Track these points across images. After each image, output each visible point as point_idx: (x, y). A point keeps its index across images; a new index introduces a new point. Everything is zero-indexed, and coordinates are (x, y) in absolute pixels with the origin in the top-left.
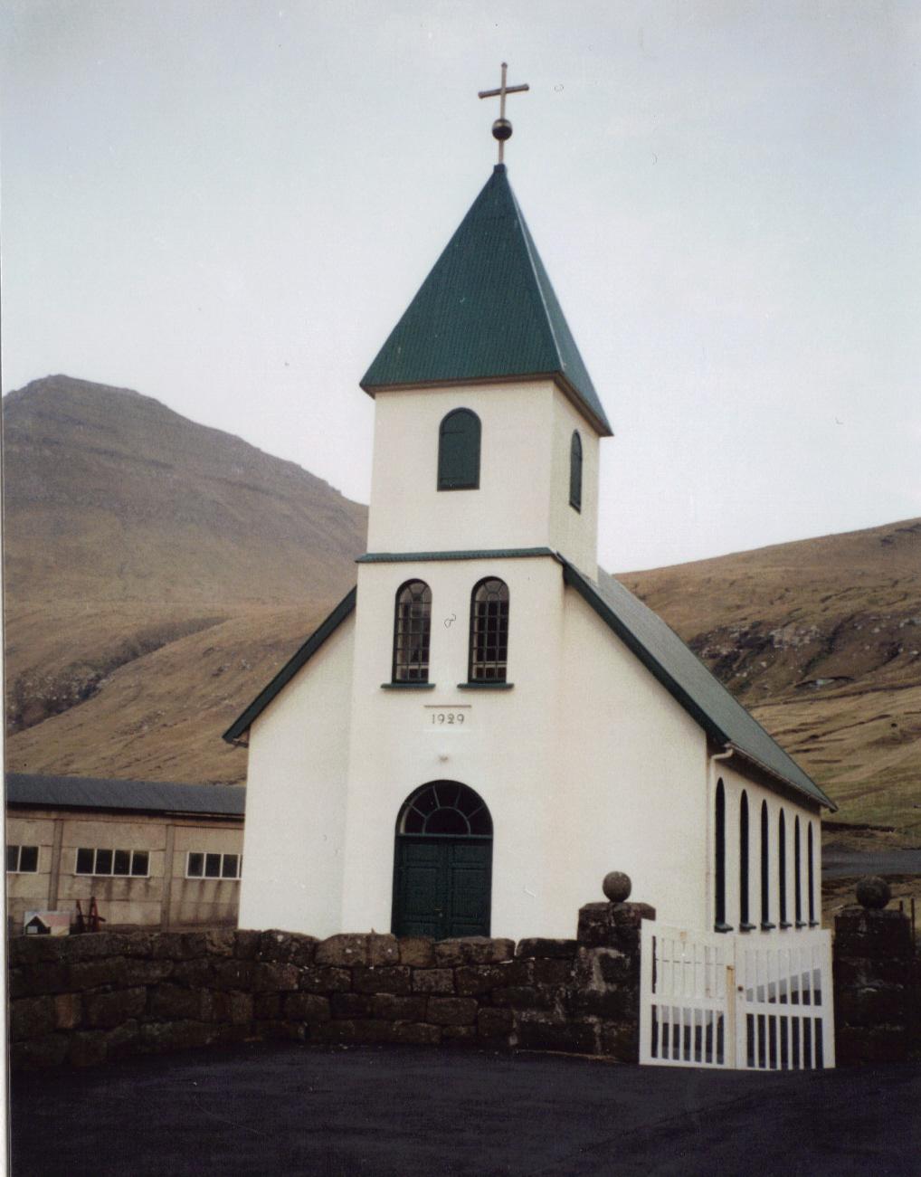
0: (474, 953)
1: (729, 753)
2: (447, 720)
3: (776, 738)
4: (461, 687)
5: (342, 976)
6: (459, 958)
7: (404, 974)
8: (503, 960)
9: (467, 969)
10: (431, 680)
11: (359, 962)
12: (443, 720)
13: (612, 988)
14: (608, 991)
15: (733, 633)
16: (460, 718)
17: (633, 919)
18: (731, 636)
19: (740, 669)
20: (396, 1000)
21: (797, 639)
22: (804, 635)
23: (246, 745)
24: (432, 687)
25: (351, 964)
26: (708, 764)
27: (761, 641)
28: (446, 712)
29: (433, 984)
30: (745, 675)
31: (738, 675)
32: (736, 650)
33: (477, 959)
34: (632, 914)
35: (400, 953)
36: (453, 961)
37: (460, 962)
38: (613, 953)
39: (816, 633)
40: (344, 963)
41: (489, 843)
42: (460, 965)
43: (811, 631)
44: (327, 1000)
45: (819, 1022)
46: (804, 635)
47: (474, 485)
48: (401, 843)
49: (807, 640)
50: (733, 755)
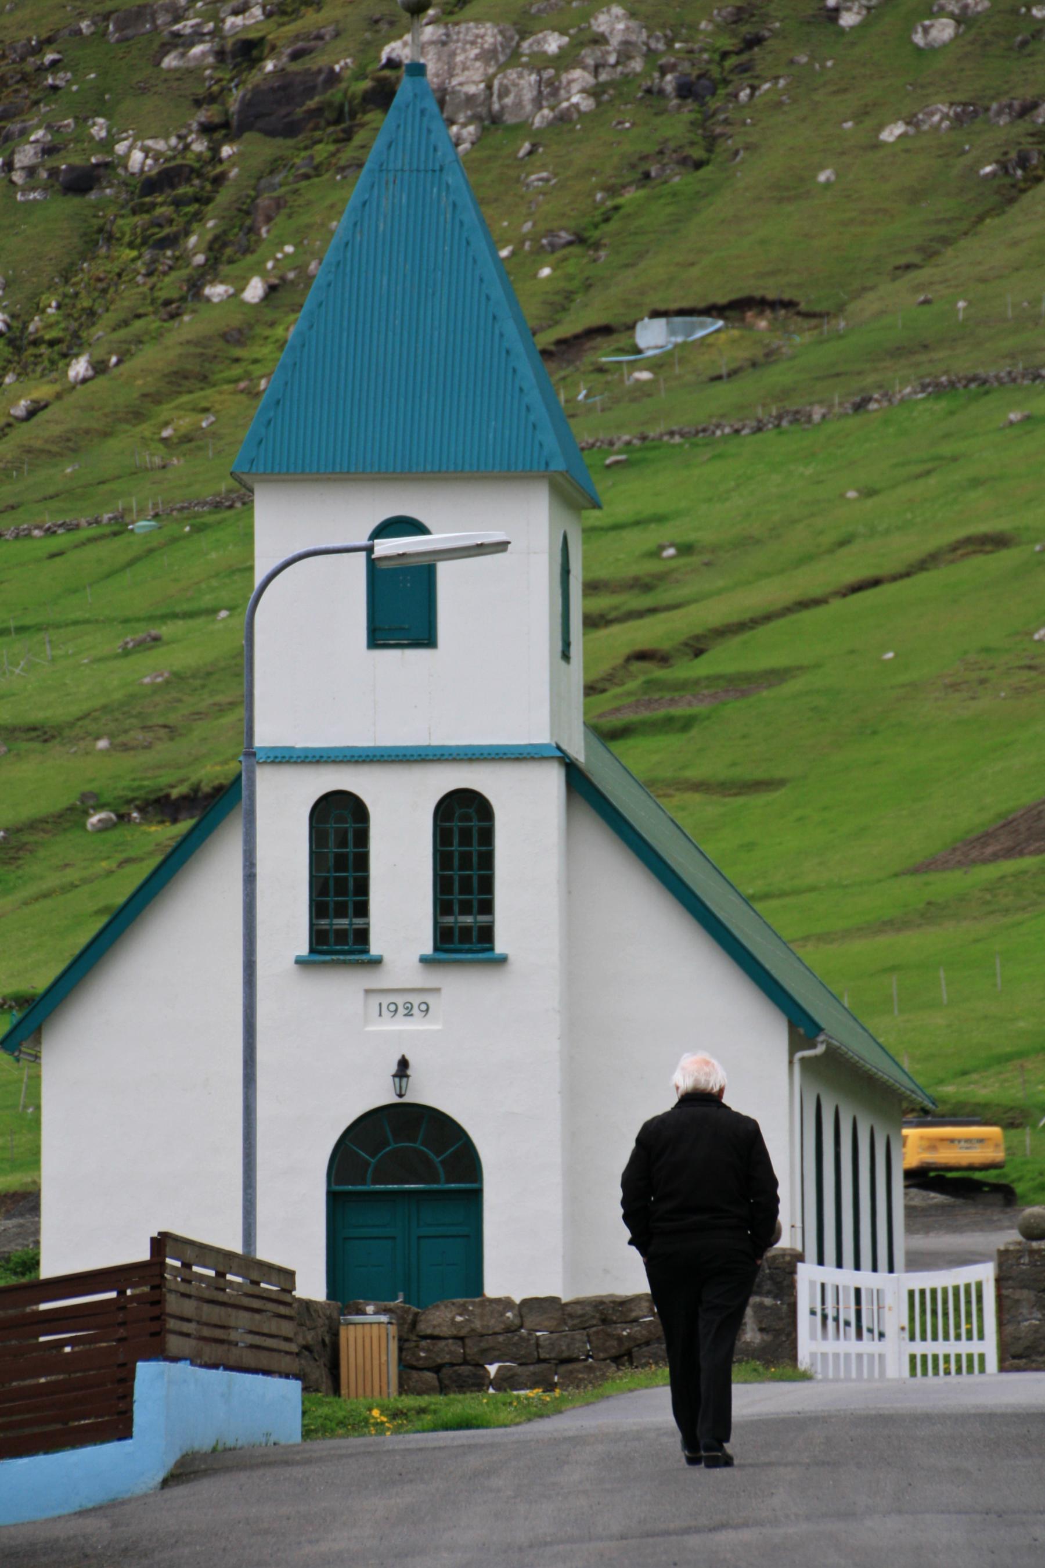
0: (610, 1312)
1: (820, 1050)
2: (401, 1011)
3: (758, 906)
4: (424, 960)
5: (453, 1348)
6: (593, 1317)
7: (529, 1340)
8: (643, 1317)
9: (602, 1330)
10: (376, 947)
11: (473, 1330)
12: (396, 1011)
13: (768, 1338)
14: (763, 1340)
15: (180, 42)
16: (423, 1007)
17: (789, 1263)
18: (170, 61)
19: (225, 255)
20: (520, 1370)
21: (526, 83)
22: (565, 60)
23: (37, 1057)
24: (377, 962)
25: (463, 1333)
26: (791, 1062)
27: (335, 95)
28: (400, 1000)
29: (564, 1348)
30: (254, 290)
31: (217, 291)
32: (199, 146)
33: (615, 1318)
34: (788, 1258)
35: (521, 1316)
36: (586, 1321)
37: (594, 1322)
38: (768, 1301)
39: (625, 53)
40: (455, 1332)
41: (475, 1196)
42: (594, 1326)
43: (600, 40)
44: (435, 1376)
45: (982, 1357)
46: (565, 60)
47: (426, 639)
48: (335, 1200)
49: (576, 90)
50: (826, 1053)
